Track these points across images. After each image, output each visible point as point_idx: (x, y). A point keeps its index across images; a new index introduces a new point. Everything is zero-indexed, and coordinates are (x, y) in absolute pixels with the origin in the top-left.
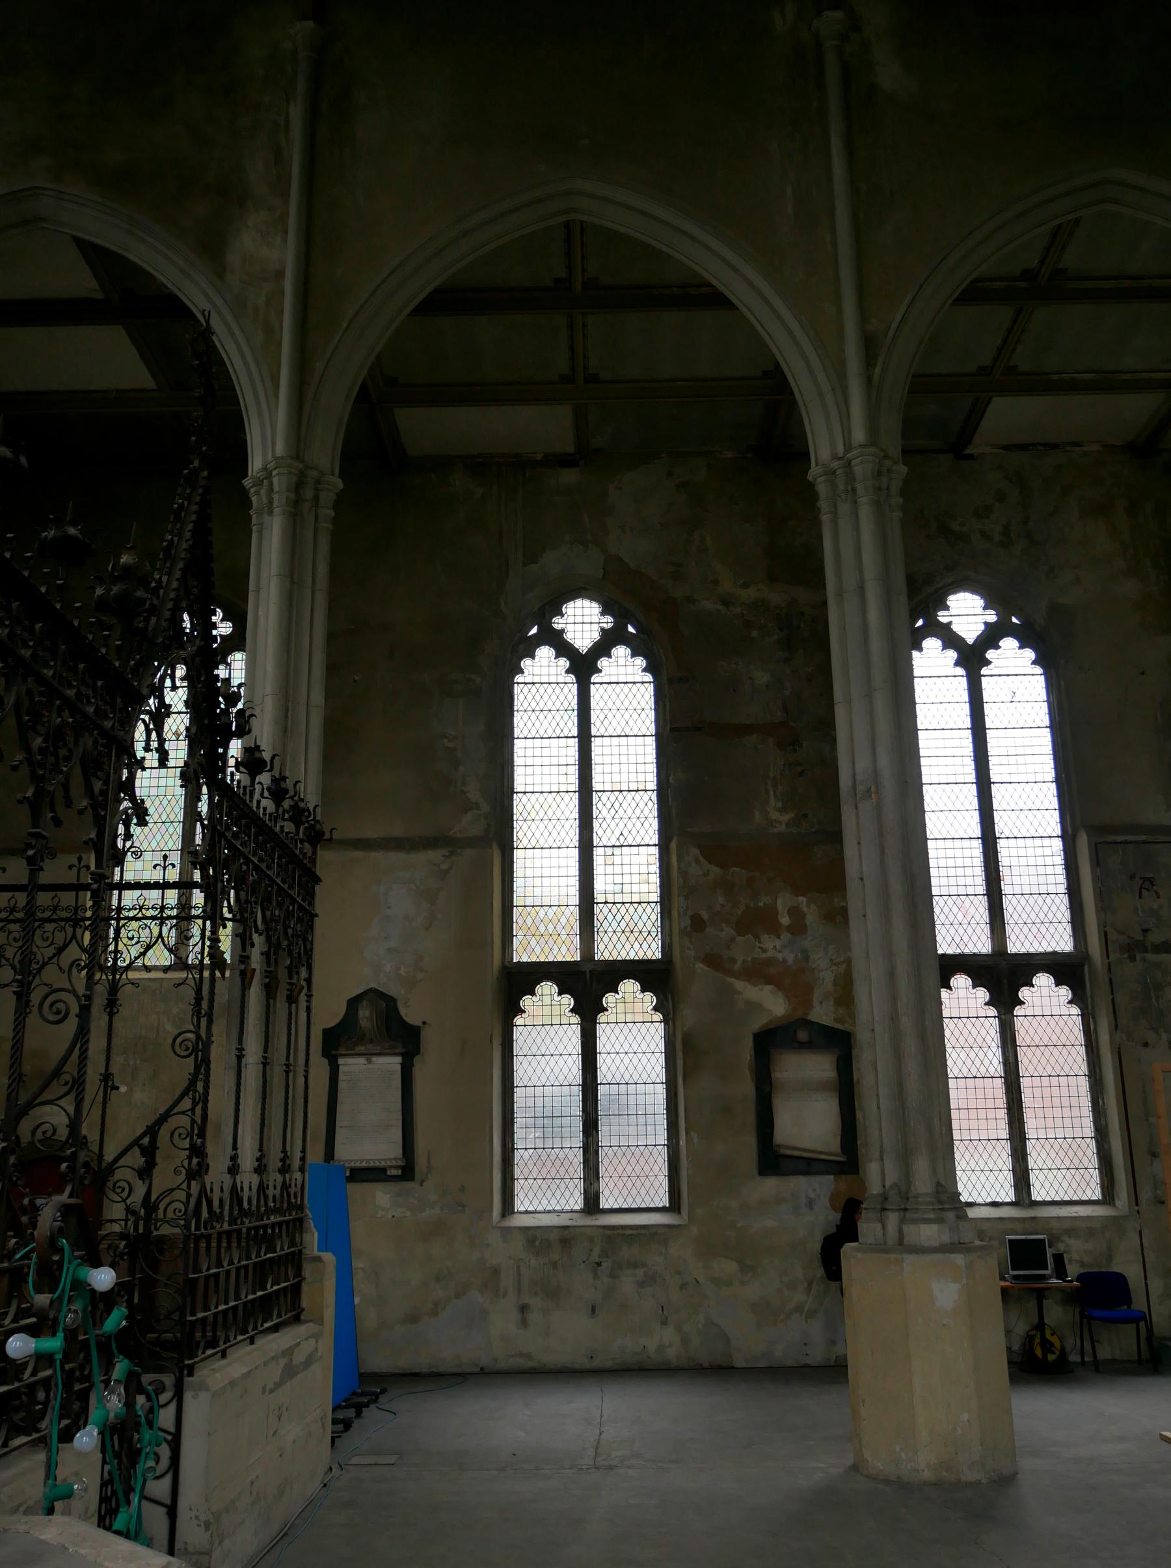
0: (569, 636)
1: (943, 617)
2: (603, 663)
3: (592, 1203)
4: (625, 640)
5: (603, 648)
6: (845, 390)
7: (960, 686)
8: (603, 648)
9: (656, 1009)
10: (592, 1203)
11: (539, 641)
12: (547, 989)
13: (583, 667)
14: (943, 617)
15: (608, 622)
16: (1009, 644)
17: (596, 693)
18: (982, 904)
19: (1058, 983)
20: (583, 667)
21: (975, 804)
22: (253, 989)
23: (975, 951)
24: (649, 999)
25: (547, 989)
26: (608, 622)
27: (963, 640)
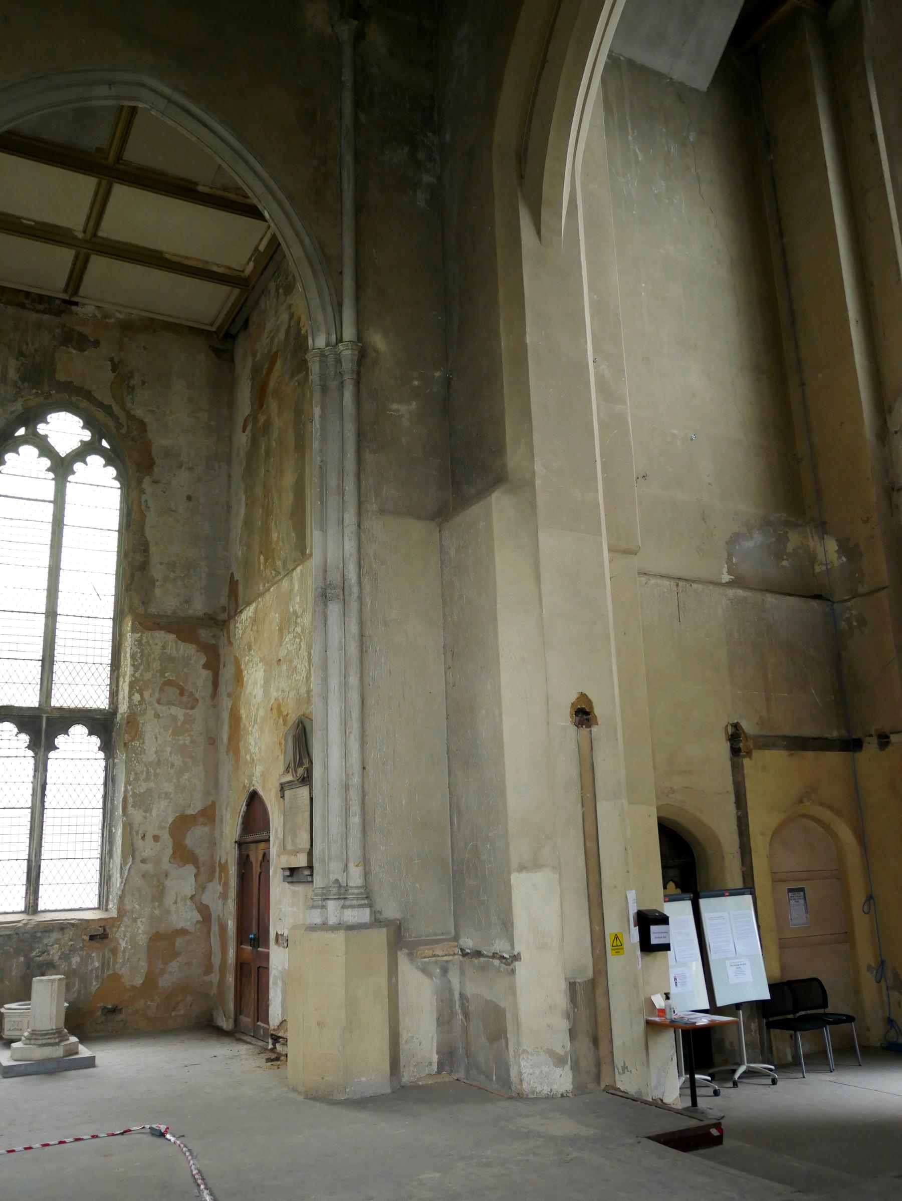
0: (51, 441)
1: (42, 429)
2: (78, 466)
3: (32, 906)
4: (101, 452)
5: (80, 454)
6: (340, 305)
7: (48, 488)
8: (80, 454)
9: (29, 747)
10: (32, 906)
11: (24, 440)
12: (79, 731)
13: (62, 467)
14: (42, 429)
15: (87, 436)
16: (95, 461)
17: (71, 489)
18: (36, 669)
19: (21, 730)
20: (62, 467)
21: (45, 585)
22: (352, 736)
23: (80, 706)
24: (95, 741)
25: (79, 731)
26: (87, 436)
27: (58, 454)
